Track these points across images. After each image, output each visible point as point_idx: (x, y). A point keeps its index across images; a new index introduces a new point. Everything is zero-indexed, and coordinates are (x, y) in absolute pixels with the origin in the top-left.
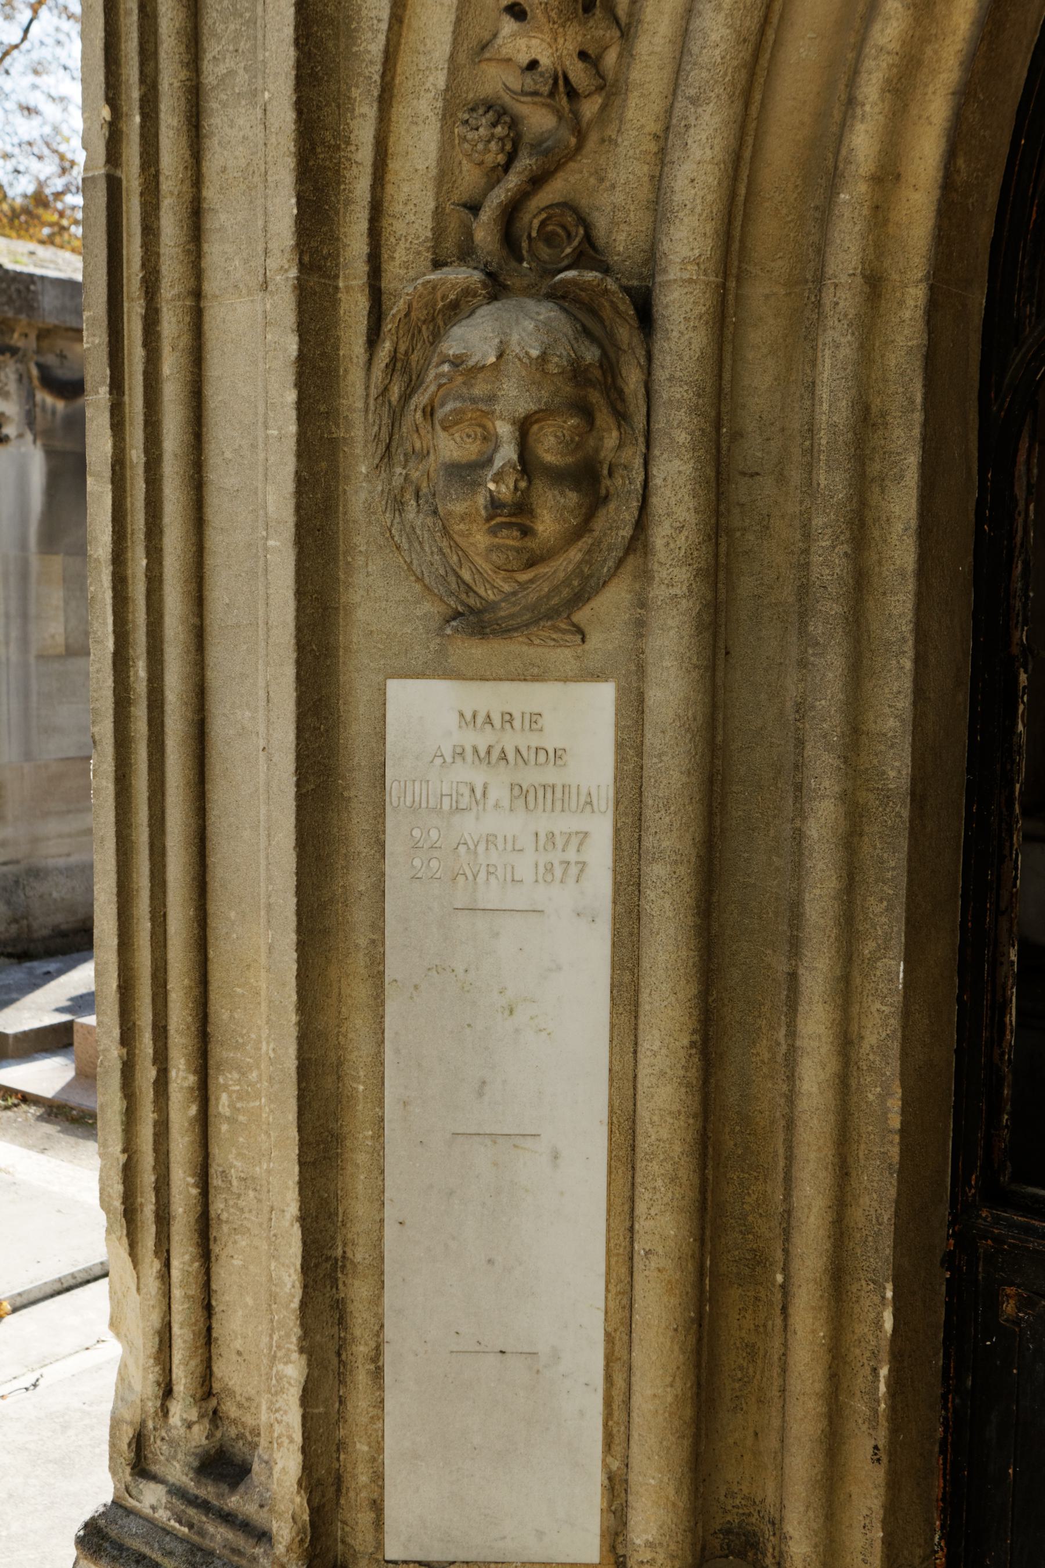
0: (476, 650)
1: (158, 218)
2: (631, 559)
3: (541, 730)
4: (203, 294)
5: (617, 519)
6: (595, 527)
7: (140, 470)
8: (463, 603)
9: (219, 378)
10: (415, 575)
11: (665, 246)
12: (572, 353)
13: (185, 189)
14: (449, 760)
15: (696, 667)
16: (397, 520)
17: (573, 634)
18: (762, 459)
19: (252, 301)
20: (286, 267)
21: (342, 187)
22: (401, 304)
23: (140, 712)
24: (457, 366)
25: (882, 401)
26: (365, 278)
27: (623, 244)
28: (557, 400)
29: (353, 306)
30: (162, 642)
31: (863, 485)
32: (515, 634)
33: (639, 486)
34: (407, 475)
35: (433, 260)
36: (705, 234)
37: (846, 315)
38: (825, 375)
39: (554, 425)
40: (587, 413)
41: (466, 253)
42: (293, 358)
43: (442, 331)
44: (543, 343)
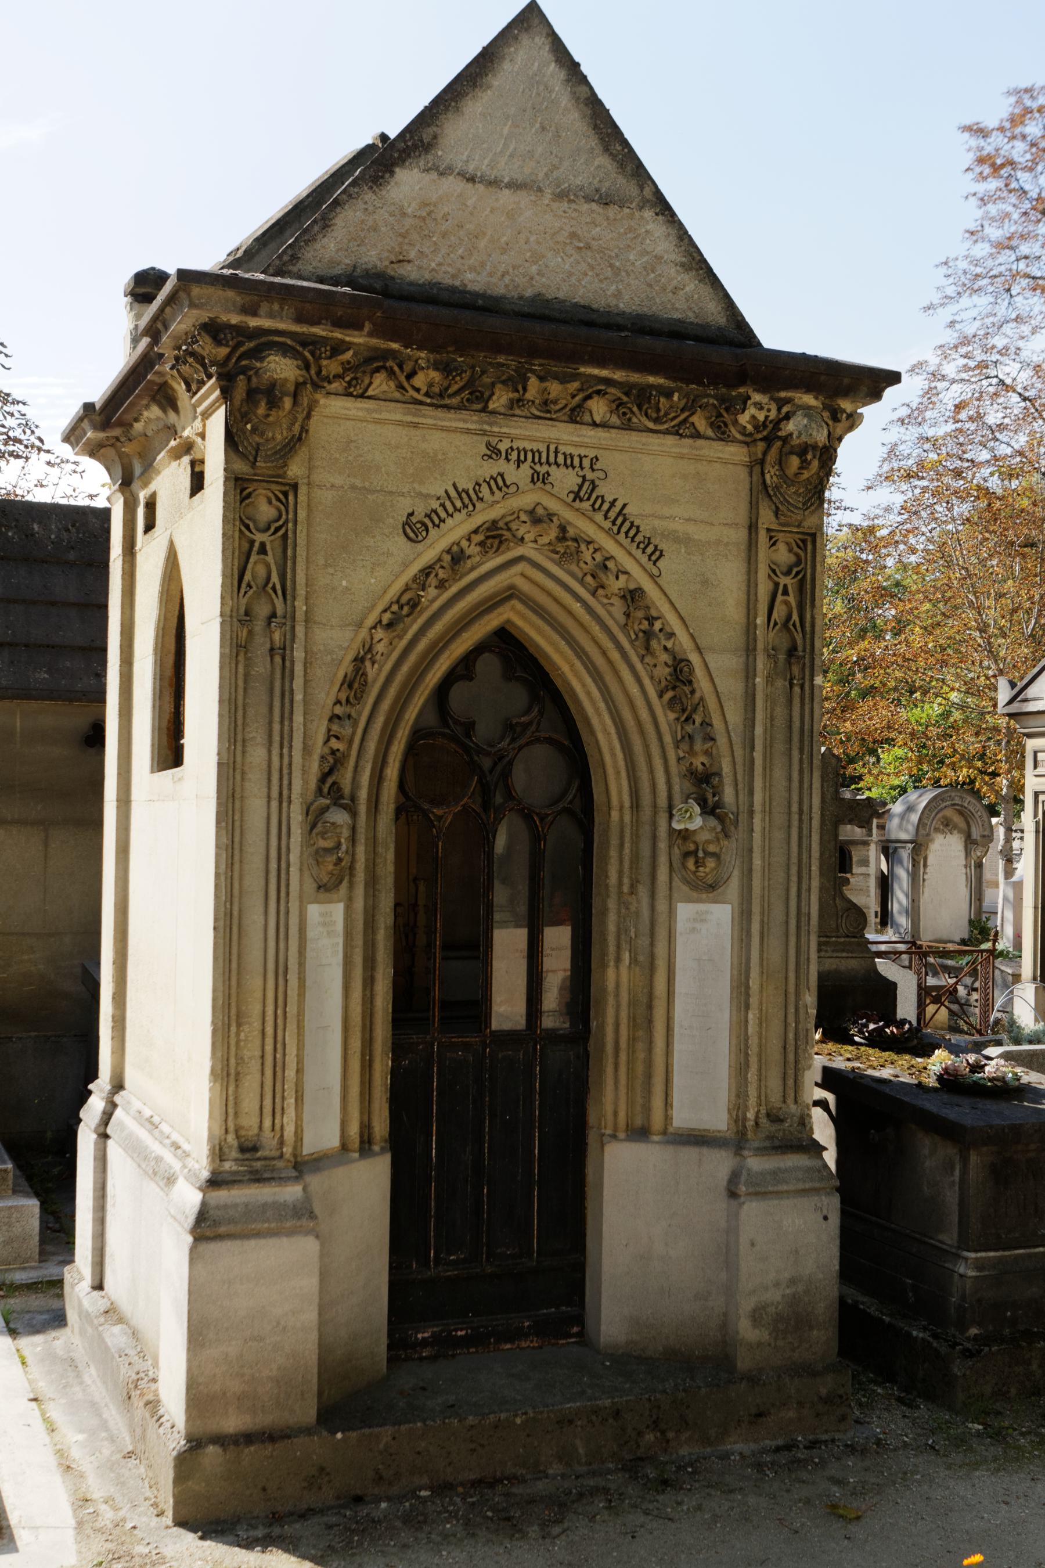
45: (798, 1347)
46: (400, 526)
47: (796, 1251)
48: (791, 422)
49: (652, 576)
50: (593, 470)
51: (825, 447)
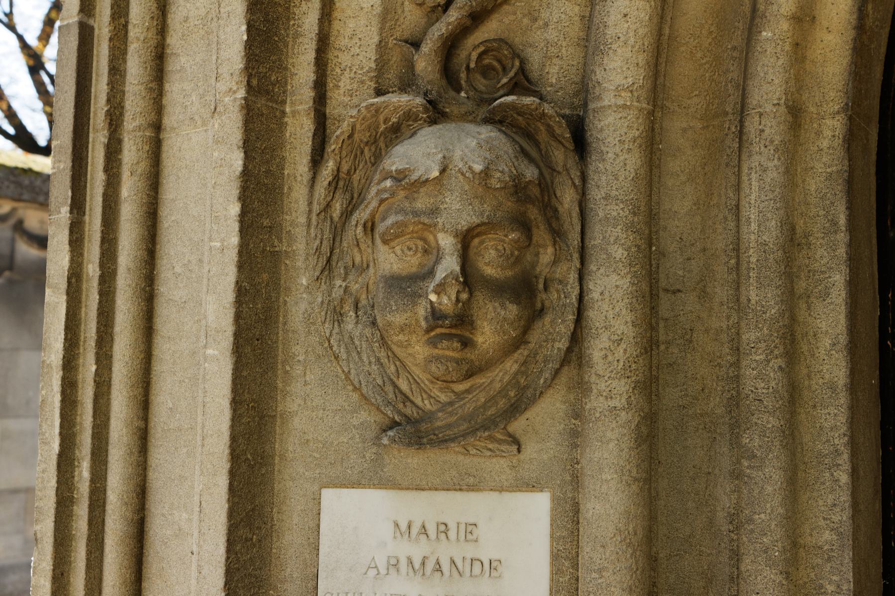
0: (413, 460)
1: (125, 61)
2: (565, 369)
3: (476, 541)
4: (163, 127)
5: (555, 330)
6: (531, 339)
7: (95, 283)
8: (399, 413)
9: (173, 200)
10: (353, 384)
11: (599, 75)
12: (513, 169)
13: (150, 35)
14: (383, 571)
15: (636, 480)
16: (336, 330)
17: (509, 444)
18: (684, 277)
19: (206, 131)
20: (235, 88)
21: (292, 23)
22: (345, 126)
23: (82, 511)
24: (400, 181)
25: (805, 223)
26: (311, 103)
27: (556, 76)
28: (499, 214)
29: (299, 129)
30: (107, 443)
31: (792, 300)
32: (452, 445)
33: (574, 300)
34: (346, 287)
35: (375, 88)
36: (638, 64)
37: (772, 142)
38: (753, 197)
39: (494, 239)
40: (525, 226)
41: (407, 84)
42: (238, 173)
43: (383, 153)
44: (486, 158)
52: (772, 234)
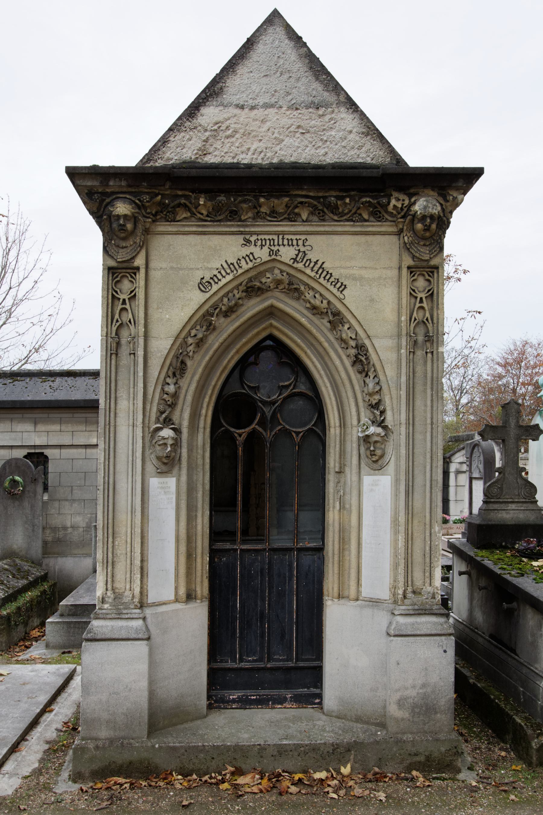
45: (428, 723)
46: (197, 285)
47: (426, 669)
48: (417, 205)
49: (340, 300)
50: (304, 245)
51: (439, 217)
52: (202, 444)
